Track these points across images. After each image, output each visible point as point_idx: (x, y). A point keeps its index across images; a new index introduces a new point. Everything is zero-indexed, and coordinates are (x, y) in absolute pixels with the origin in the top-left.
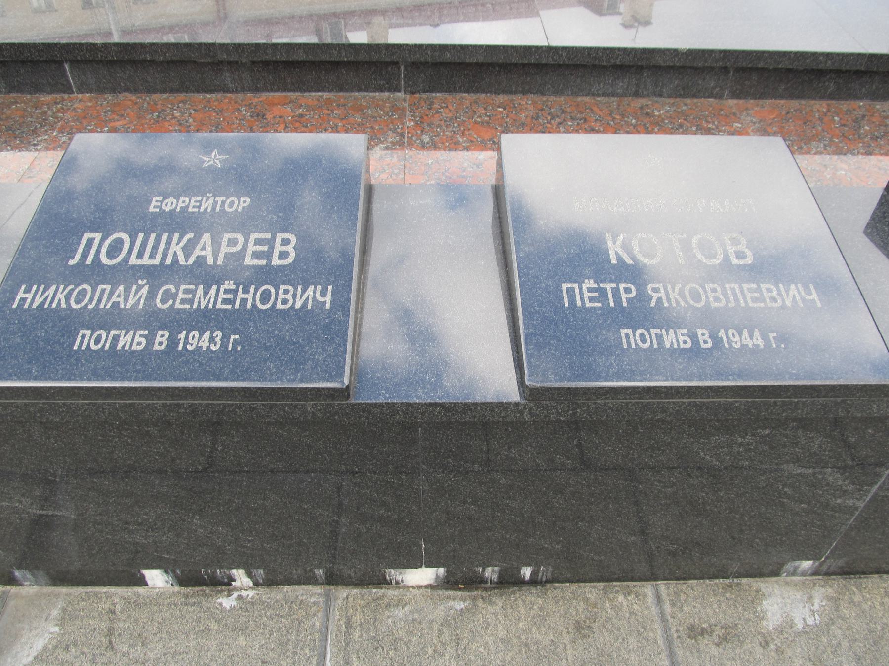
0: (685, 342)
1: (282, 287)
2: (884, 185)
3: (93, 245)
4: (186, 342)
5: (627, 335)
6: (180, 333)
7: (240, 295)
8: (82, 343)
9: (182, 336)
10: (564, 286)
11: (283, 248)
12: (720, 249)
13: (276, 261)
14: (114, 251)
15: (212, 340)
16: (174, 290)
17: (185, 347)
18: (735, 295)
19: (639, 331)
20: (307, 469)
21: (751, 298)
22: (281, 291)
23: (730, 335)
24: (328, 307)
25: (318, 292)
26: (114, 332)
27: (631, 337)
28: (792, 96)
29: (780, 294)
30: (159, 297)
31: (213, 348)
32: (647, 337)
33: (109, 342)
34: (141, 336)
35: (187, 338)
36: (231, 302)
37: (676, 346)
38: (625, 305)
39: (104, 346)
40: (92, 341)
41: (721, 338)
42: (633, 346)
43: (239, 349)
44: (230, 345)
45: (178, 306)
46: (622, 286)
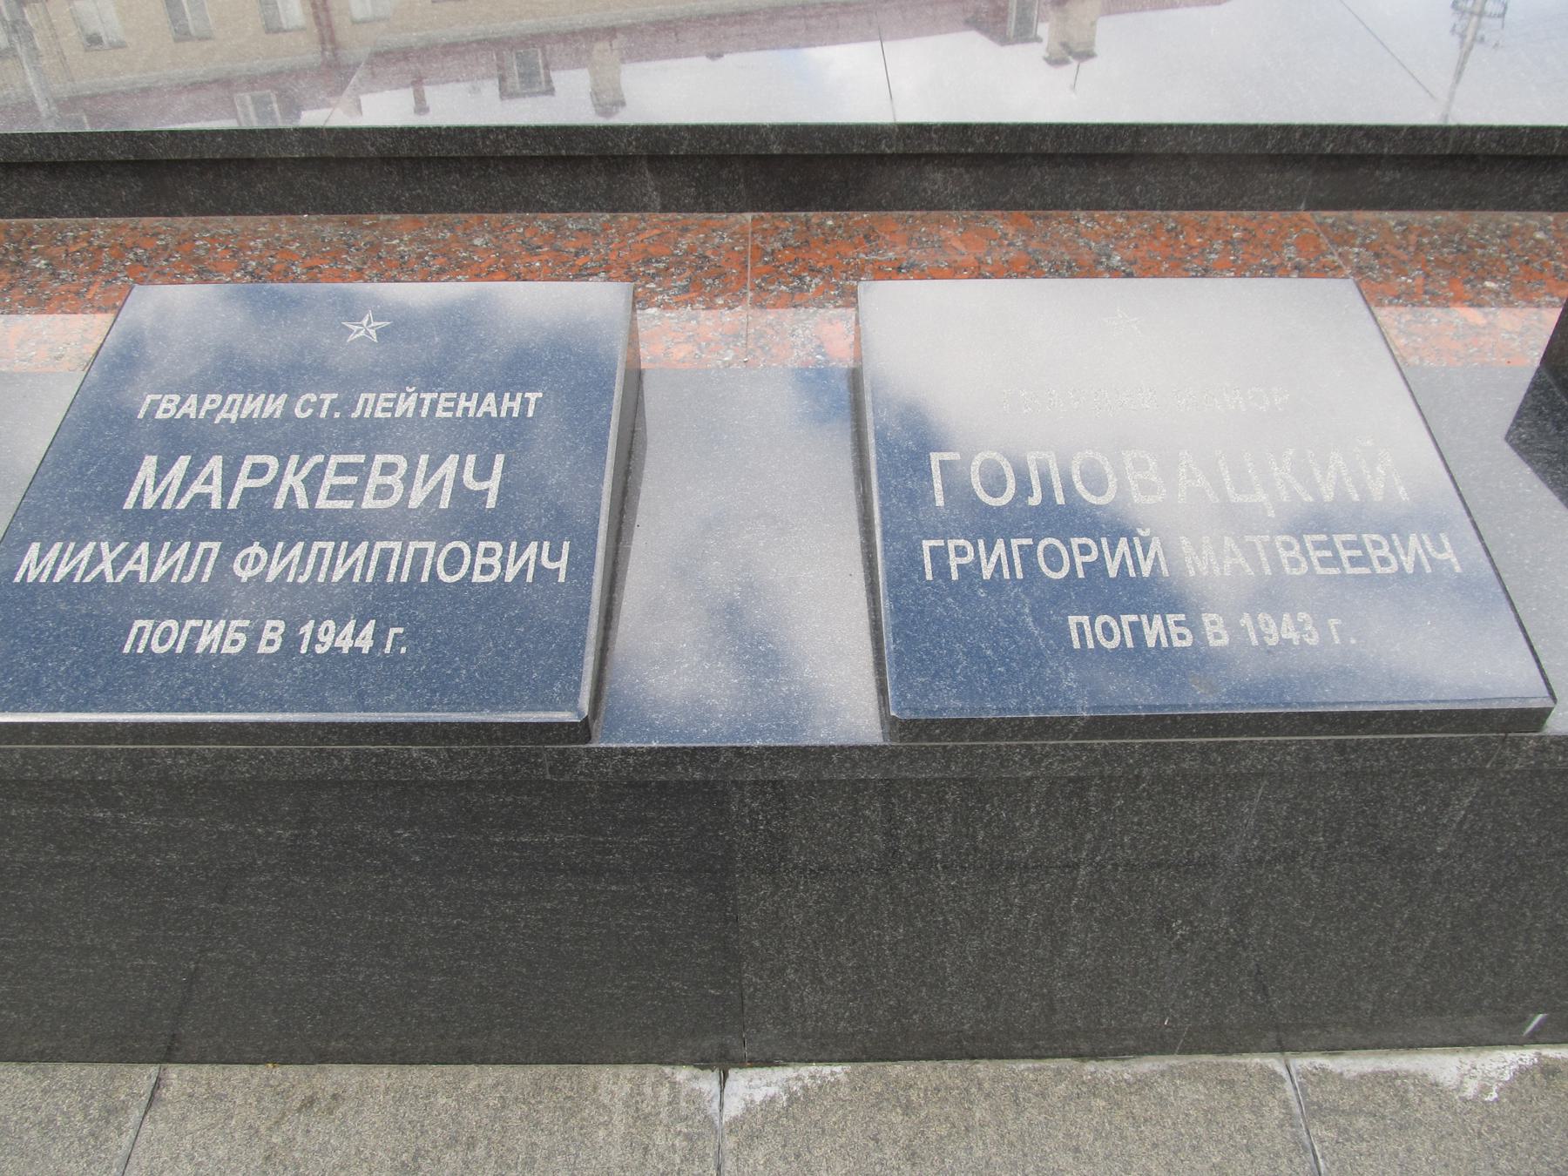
1: (482, 545)
4: (314, 640)
5: (1080, 626)
6: (304, 622)
8: (1082, 634)
9: (307, 630)
10: (927, 544)
12: (1254, 474)
13: (368, 502)
15: (1299, 627)
19: (1101, 619)
20: (518, 857)
21: (1320, 560)
25: (545, 554)
26: (191, 623)
28: (1317, 205)
32: (1116, 630)
34: (238, 630)
35: (315, 632)
38: (955, 576)
40: (155, 642)
41: (1245, 628)
42: (1091, 645)
43: (403, 650)
46: (951, 544)
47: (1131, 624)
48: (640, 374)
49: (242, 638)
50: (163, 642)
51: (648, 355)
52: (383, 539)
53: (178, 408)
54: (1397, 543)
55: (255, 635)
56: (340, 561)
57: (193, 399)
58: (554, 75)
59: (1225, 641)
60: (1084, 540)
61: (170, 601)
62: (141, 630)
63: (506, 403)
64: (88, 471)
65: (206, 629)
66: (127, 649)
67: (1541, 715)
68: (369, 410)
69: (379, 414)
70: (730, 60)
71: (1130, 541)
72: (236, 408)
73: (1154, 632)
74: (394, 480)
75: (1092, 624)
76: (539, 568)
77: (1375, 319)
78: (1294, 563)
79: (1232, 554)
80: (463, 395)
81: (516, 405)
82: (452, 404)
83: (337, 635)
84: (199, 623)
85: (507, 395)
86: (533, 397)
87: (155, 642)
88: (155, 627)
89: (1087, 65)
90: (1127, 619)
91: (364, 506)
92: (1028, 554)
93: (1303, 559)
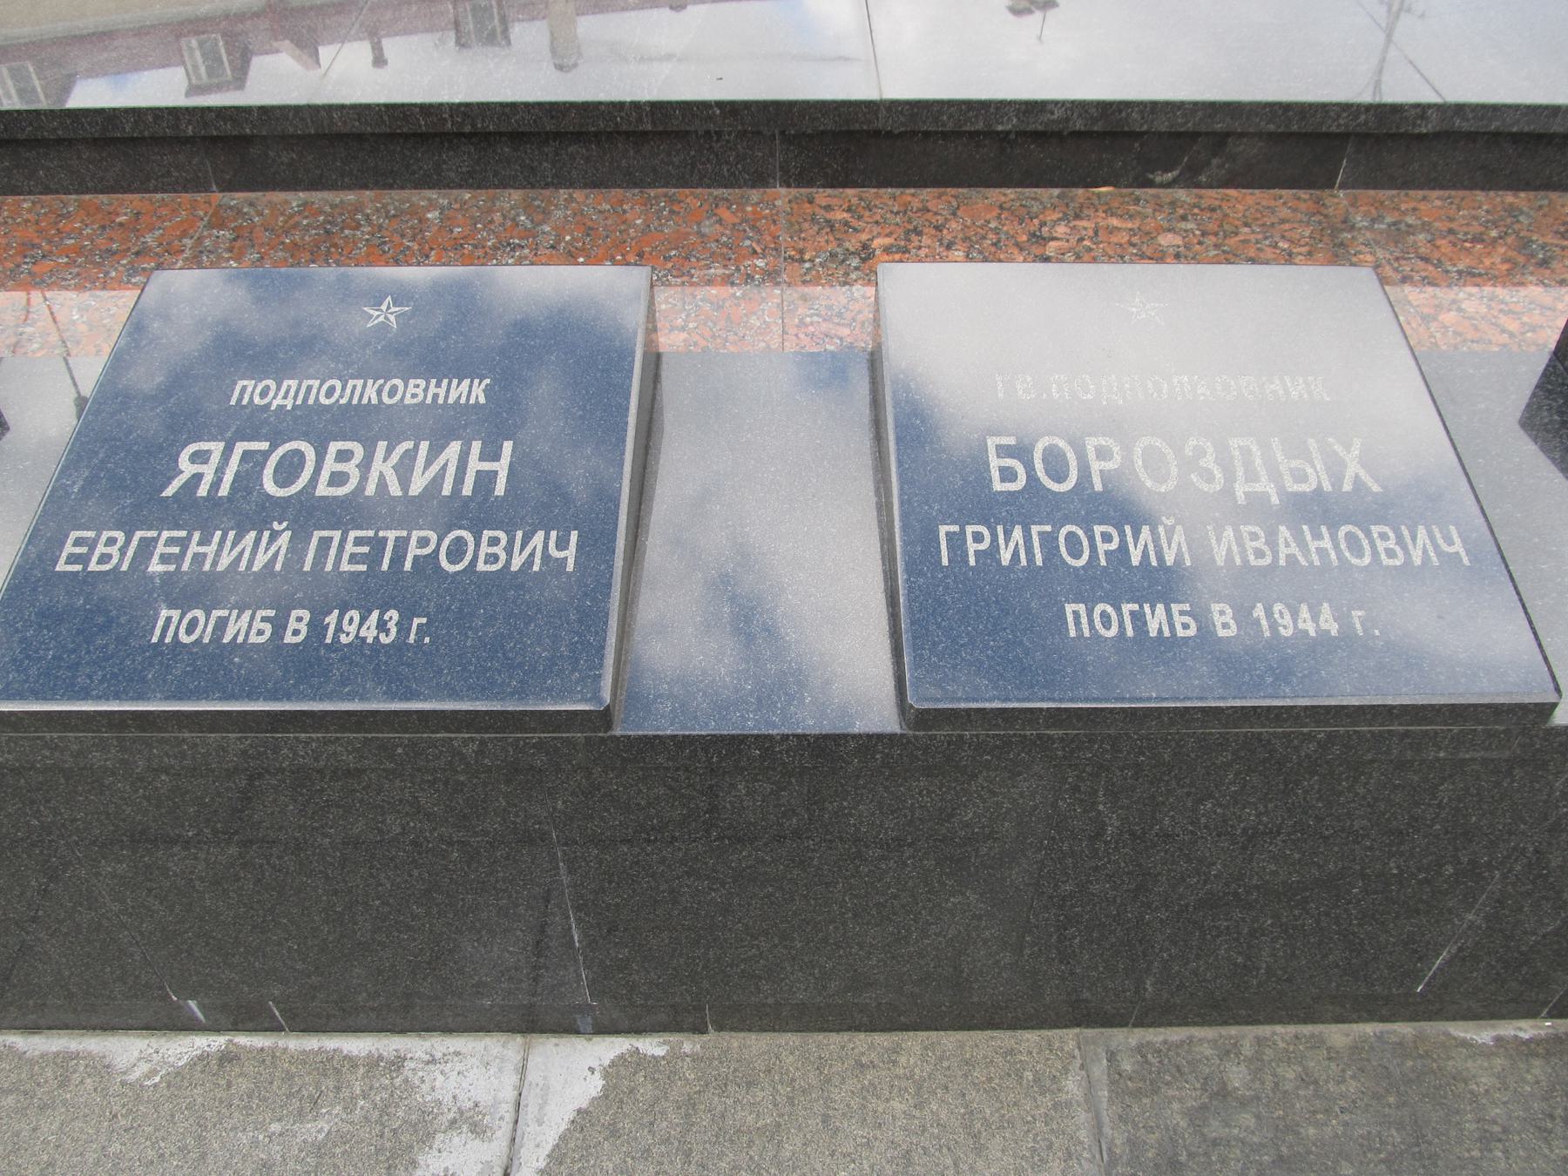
0: (1186, 626)
1: (487, 534)
2: (1552, 338)
3: (204, 466)
4: (339, 629)
5: (1076, 614)
6: (329, 613)
7: (194, 548)
9: (332, 619)
11: (340, 467)
12: (1259, 457)
15: (382, 626)
22: (485, 539)
24: (570, 567)
25: (552, 544)
27: (1084, 620)
30: (1063, 549)
31: (384, 640)
33: (210, 629)
34: (264, 619)
36: (83, 559)
37: (1167, 633)
38: (972, 562)
39: (201, 637)
40: (182, 630)
41: (1258, 620)
43: (427, 640)
46: (970, 529)
47: (1132, 613)
48: (659, 356)
49: (268, 628)
50: (189, 632)
51: (668, 341)
54: (1406, 533)
55: (279, 625)
59: (1232, 631)
61: (196, 591)
63: (432, 390)
64: (119, 457)
67: (1547, 709)
68: (301, 397)
71: (1154, 532)
72: (292, 393)
73: (1156, 620)
74: (351, 468)
76: (546, 557)
78: (1390, 553)
87: (182, 630)
90: (1127, 608)
91: (318, 493)
92: (1049, 541)
93: (1398, 549)
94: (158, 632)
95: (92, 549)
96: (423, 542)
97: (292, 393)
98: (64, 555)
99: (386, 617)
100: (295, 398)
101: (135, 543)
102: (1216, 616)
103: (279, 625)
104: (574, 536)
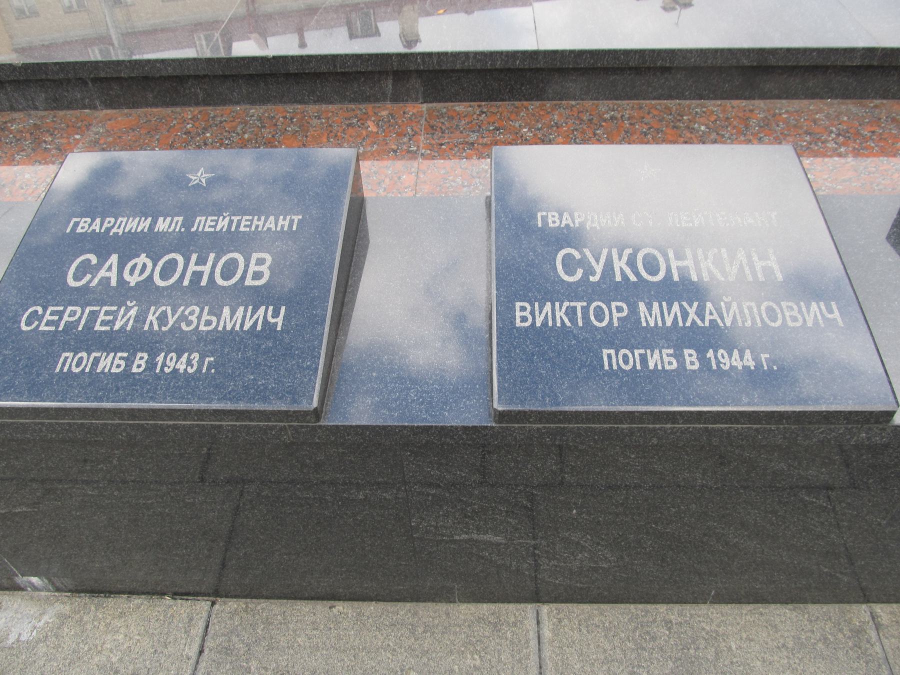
1: (614, 305)
4: (164, 365)
5: (609, 356)
8: (64, 364)
14: (231, 266)
15: (189, 363)
16: (40, 312)
17: (162, 370)
18: (751, 313)
23: (719, 355)
24: (279, 329)
25: (270, 313)
29: (800, 311)
31: (190, 370)
32: (621, 362)
33: (89, 365)
34: (121, 358)
35: (165, 358)
36: (56, 324)
37: (660, 368)
39: (84, 370)
42: (615, 367)
43: (213, 371)
44: (205, 366)
45: (43, 328)
47: (640, 355)
49: (123, 363)
52: (70, 305)
53: (90, 225)
54: (804, 309)
55: (129, 361)
56: (550, 314)
57: (98, 221)
58: (379, 24)
60: (619, 304)
62: (67, 358)
63: (281, 222)
65: (103, 358)
66: (58, 370)
67: (890, 414)
69: (207, 229)
70: (477, 15)
72: (122, 226)
75: (617, 355)
77: (802, 164)
78: (794, 319)
79: (711, 314)
80: (256, 218)
81: (287, 223)
82: (249, 223)
83: (176, 362)
84: (98, 354)
85: (281, 217)
86: (296, 218)
88: (74, 356)
89: (687, 12)
94: (59, 366)
95: (61, 319)
96: (72, 314)
97: (122, 226)
98: (99, 321)
99: (192, 357)
100: (124, 229)
101: (86, 315)
102: (687, 357)
103: (129, 361)
104: (283, 309)
